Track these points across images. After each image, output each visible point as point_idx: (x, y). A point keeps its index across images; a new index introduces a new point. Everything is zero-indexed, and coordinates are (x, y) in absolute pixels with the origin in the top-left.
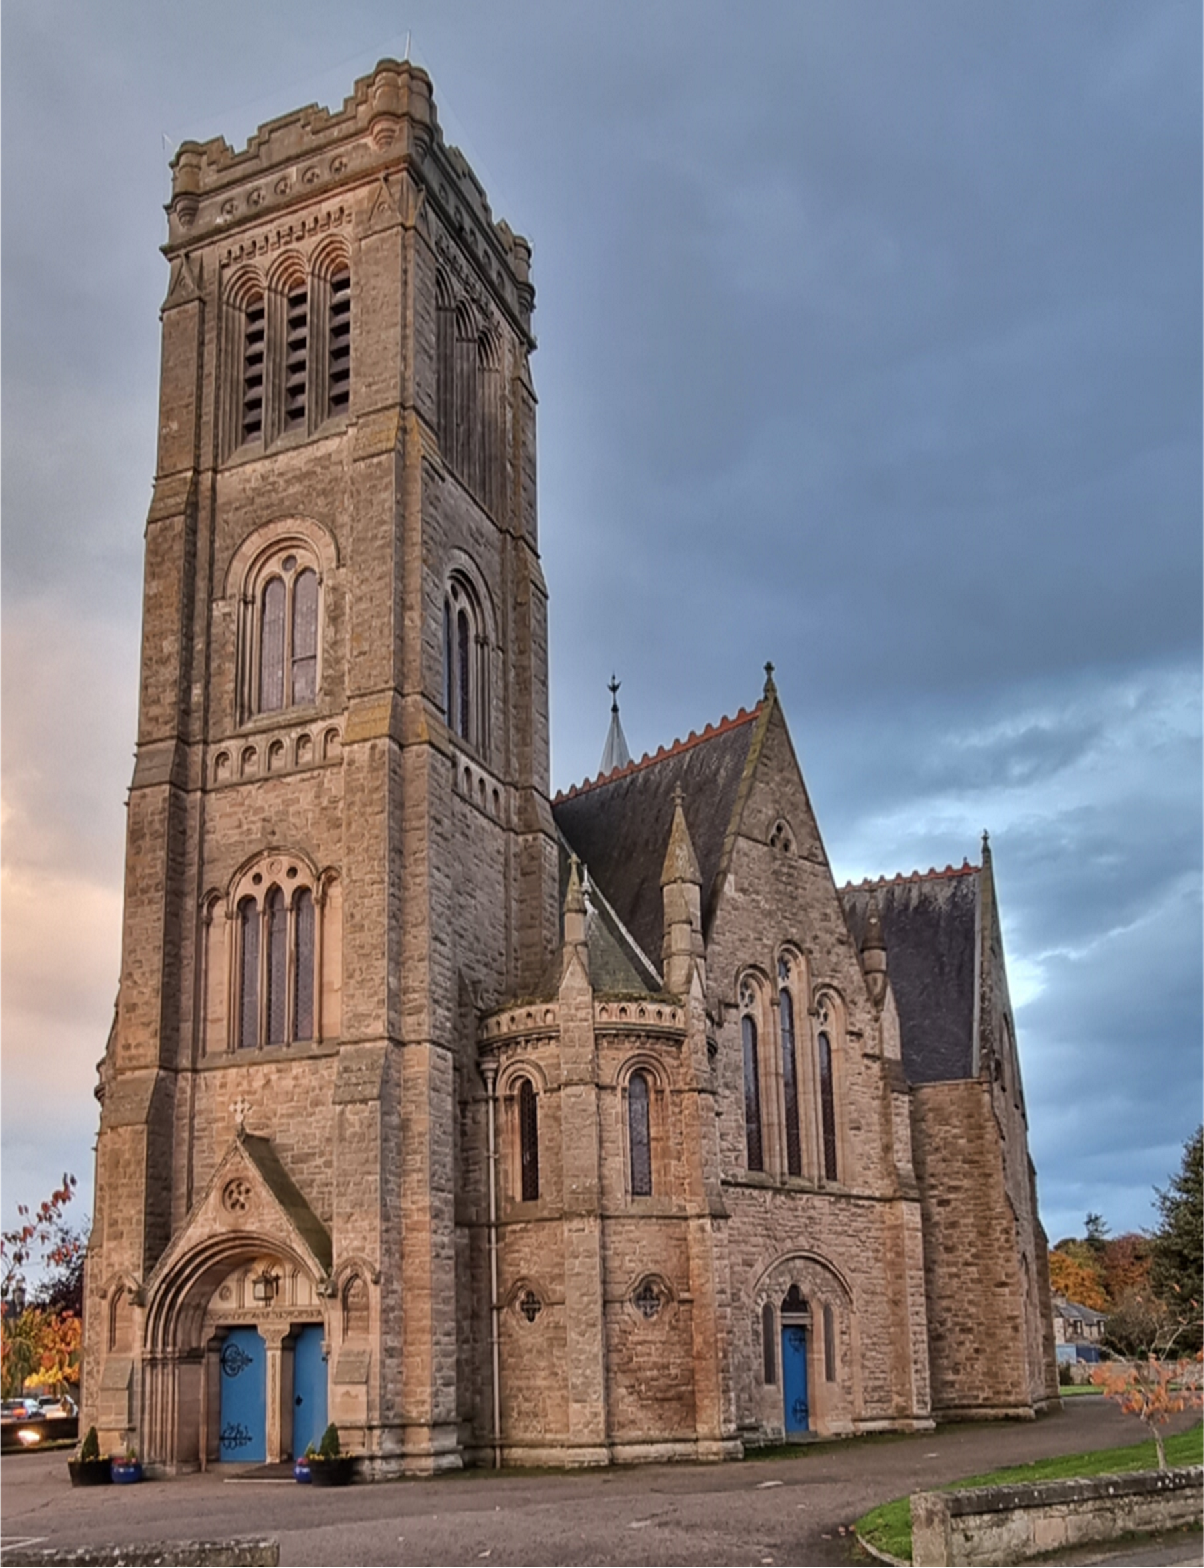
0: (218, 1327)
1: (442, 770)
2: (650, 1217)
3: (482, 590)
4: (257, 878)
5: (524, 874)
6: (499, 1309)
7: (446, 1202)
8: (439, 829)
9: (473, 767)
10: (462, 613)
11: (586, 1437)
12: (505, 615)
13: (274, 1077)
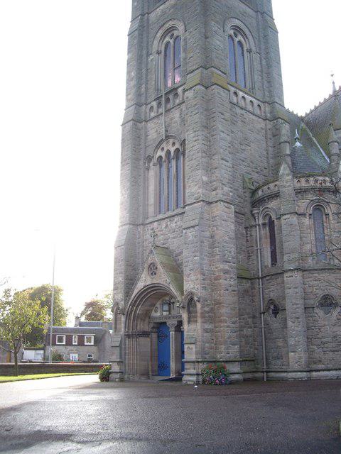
0: (155, 323)
1: (223, 94)
2: (325, 269)
3: (247, 32)
4: (163, 149)
5: (274, 136)
6: (264, 313)
7: (231, 267)
8: (223, 117)
9: (246, 96)
10: (240, 42)
11: (296, 368)
12: (259, 41)
13: (169, 223)
